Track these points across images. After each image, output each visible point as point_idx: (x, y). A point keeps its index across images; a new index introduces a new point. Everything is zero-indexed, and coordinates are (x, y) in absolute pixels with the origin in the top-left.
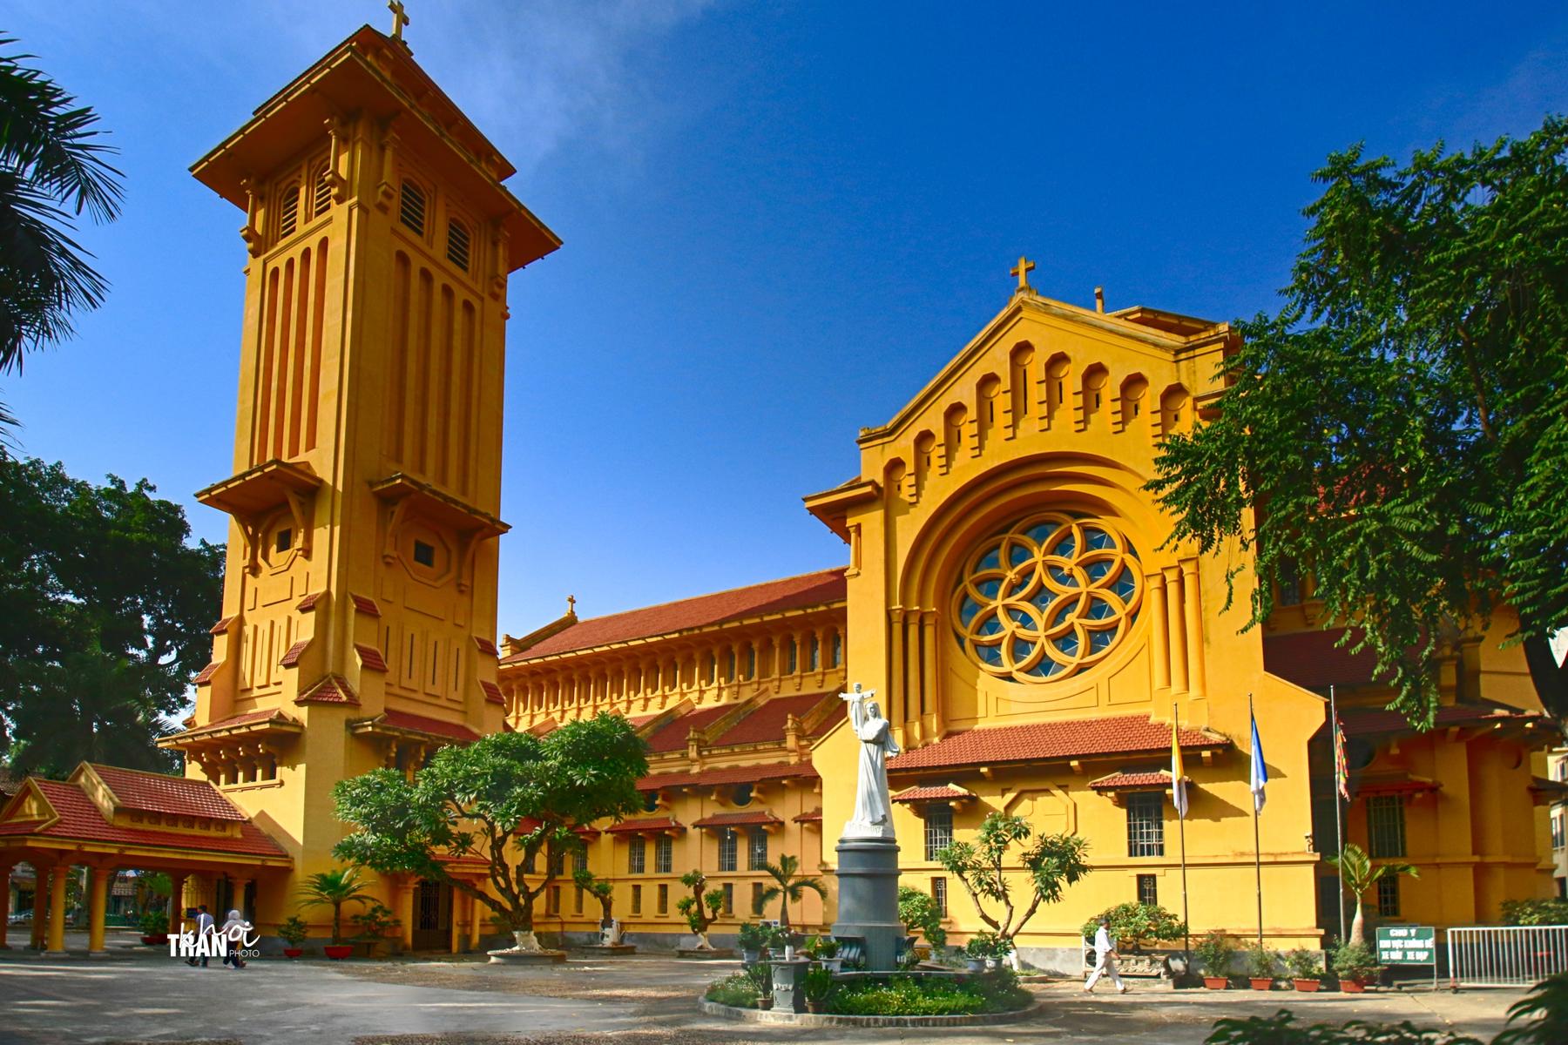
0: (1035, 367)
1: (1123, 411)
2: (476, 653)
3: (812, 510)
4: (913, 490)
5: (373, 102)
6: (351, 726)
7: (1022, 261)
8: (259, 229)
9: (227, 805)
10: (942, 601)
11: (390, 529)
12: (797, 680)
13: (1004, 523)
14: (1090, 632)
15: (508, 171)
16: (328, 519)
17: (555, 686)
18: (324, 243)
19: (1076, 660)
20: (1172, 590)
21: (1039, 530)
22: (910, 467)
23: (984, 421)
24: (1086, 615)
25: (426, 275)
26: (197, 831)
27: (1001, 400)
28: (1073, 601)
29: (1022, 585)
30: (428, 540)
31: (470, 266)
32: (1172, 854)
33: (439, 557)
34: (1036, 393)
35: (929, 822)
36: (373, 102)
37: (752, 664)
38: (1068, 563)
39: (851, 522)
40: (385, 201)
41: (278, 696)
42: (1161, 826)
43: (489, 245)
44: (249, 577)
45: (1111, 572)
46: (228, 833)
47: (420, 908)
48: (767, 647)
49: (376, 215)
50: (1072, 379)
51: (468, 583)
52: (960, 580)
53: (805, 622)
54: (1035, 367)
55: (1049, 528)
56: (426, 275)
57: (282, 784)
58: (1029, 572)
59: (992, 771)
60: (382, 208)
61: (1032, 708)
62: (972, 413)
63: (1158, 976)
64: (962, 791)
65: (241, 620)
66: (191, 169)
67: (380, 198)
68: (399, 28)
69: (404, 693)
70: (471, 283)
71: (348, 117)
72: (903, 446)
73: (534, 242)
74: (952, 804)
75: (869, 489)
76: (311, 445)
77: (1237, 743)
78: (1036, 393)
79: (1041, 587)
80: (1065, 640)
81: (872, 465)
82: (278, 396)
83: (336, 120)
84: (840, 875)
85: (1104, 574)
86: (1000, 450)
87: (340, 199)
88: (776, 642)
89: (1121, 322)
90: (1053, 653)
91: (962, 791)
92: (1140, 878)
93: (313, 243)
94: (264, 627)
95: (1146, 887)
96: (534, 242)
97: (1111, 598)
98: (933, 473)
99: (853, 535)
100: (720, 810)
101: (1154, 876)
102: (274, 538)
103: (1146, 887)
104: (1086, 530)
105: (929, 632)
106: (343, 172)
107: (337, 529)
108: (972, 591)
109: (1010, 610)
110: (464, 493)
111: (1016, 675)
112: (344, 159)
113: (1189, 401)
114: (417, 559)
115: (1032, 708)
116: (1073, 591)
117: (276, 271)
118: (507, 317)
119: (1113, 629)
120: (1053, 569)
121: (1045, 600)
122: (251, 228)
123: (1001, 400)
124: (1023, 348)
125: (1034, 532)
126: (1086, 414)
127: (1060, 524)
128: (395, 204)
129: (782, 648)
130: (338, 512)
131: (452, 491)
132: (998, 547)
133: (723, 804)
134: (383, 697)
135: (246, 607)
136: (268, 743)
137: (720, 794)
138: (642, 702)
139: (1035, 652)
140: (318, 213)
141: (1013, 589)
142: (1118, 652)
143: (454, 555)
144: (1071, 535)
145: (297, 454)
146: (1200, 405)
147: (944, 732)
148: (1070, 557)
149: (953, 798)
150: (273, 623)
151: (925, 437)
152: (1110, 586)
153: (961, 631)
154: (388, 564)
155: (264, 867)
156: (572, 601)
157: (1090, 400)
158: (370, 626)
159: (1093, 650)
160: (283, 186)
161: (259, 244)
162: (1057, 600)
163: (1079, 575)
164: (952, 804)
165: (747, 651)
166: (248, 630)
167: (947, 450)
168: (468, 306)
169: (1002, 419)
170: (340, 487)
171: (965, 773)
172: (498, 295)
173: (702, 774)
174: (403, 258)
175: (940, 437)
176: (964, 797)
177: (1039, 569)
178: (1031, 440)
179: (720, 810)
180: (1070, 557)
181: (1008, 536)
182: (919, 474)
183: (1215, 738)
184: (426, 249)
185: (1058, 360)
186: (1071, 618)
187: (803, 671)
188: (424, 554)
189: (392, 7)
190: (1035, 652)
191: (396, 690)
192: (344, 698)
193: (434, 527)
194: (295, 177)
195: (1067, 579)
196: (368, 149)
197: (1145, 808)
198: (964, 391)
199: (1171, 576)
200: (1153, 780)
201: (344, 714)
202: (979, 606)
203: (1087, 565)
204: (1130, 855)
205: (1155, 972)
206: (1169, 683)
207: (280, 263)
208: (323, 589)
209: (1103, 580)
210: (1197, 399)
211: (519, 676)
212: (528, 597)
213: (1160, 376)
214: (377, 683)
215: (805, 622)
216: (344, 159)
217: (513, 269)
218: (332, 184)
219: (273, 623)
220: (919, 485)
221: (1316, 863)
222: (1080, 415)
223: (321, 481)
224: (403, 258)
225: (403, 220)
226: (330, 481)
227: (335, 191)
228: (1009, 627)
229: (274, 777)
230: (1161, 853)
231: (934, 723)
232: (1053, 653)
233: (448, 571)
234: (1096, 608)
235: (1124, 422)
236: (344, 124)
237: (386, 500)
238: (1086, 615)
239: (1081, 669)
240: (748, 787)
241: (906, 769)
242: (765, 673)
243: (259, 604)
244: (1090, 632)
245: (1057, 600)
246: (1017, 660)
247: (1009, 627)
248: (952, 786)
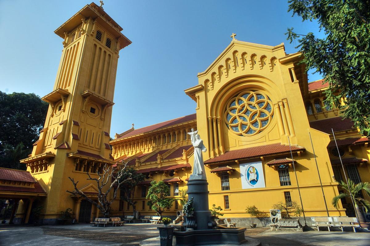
0: (239, 56)
1: (262, 64)
2: (104, 136)
3: (186, 93)
4: (212, 87)
5: (93, 15)
6: (68, 154)
7: (233, 34)
8: (66, 42)
9: (33, 179)
10: (222, 115)
11: (85, 103)
12: (187, 141)
13: (236, 94)
14: (261, 121)
15: (121, 29)
16: (70, 100)
17: (127, 145)
18: (79, 43)
19: (259, 129)
20: (281, 107)
21: (244, 95)
22: (211, 81)
23: (228, 68)
24: (260, 116)
25: (100, 49)
26: (21, 186)
27: (231, 64)
28: (256, 113)
29: (242, 110)
30: (94, 107)
31: (111, 47)
32: (294, 184)
33: (96, 111)
34: (240, 61)
35: (222, 178)
36: (93, 15)
37: (175, 138)
38: (254, 103)
39: (197, 95)
40: (93, 34)
41: (51, 148)
42: (288, 175)
43: (116, 43)
44: (51, 117)
45: (265, 105)
46: (30, 187)
47: (83, 210)
48: (179, 133)
49: (90, 37)
50: (248, 57)
51: (103, 118)
52: (226, 109)
53: (187, 124)
54: (239, 56)
56: (100, 49)
57: (48, 172)
59: (239, 161)
60: (92, 35)
61: (248, 143)
62: (225, 67)
63: (297, 227)
64: (231, 168)
65: (47, 129)
66: (54, 32)
67: (91, 33)
68: (101, 5)
69: (84, 146)
70: (111, 51)
71: (87, 18)
72: (209, 76)
73: (125, 42)
74: (228, 172)
75: (200, 87)
76: (69, 85)
77: (306, 149)
78: (240, 61)
79: (247, 110)
80: (255, 123)
81: (201, 81)
82: (64, 76)
83: (84, 19)
84: (188, 185)
85: (263, 105)
86: (232, 75)
87: (83, 34)
88: (181, 131)
90: (252, 127)
91: (231, 168)
92: (285, 192)
93: (76, 43)
94: (52, 130)
95: (287, 196)
96: (125, 42)
97: (266, 112)
98: (216, 82)
99: (197, 99)
100: (166, 178)
102: (58, 108)
103: (287, 196)
104: (257, 95)
106: (84, 29)
107: (72, 103)
108: (229, 111)
110: (104, 95)
111: (243, 134)
112: (85, 25)
113: (277, 60)
114: (91, 112)
115: (248, 143)
116: (255, 110)
117: (68, 50)
118: (119, 58)
121: (248, 113)
122: (65, 42)
123: (231, 64)
124: (235, 52)
125: (243, 96)
126: (253, 65)
128: (95, 35)
129: (183, 133)
130: (72, 100)
131: (101, 95)
132: (235, 100)
133: (166, 176)
134: (78, 147)
135: (49, 125)
136: (46, 160)
137: (165, 173)
138: (148, 149)
139: (247, 127)
140: (78, 38)
142: (269, 126)
143: (100, 111)
144: (253, 96)
145: (66, 88)
146: (281, 61)
147: (225, 151)
148: (254, 102)
149: (228, 170)
150: (54, 128)
151: (214, 74)
152: (265, 108)
153: (227, 123)
154: (83, 113)
155: (38, 196)
156: (133, 125)
157: (253, 63)
158: (77, 128)
159: (262, 126)
160: (73, 33)
161: (66, 45)
162: (252, 113)
163: (257, 106)
164: (228, 172)
165: (174, 134)
166: (48, 131)
167: (220, 76)
168: (110, 55)
169: (232, 68)
170: (73, 95)
171: (232, 163)
172: (117, 53)
173: (162, 168)
174: (95, 45)
175: (217, 73)
176: (231, 170)
177: (246, 105)
178: (240, 72)
179: (166, 178)
180: (254, 102)
181: (237, 97)
182: (213, 82)
183: (300, 147)
184: (101, 44)
185: (244, 54)
186: (256, 117)
188: (93, 111)
189: (100, 2)
190: (247, 127)
191: (82, 145)
192: (67, 147)
193: (96, 102)
194: (75, 31)
196: (90, 24)
197: (283, 170)
198: (222, 62)
199: (281, 104)
200: (285, 161)
201: (66, 152)
203: (258, 103)
204: (281, 185)
205: (296, 226)
206: (285, 133)
207: (69, 48)
208: (66, 119)
209: (263, 107)
210: (279, 59)
211: (118, 144)
212: (119, 124)
213: (269, 55)
214: (77, 143)
215: (187, 124)
216: (85, 25)
217: (121, 48)
218: (82, 31)
219: (54, 128)
220: (213, 85)
221: (338, 185)
222: (251, 66)
223: (70, 93)
224: (95, 45)
225: (96, 38)
226: (72, 94)
227: (82, 32)
228: (240, 121)
229: (46, 170)
230: (290, 184)
231: (221, 148)
232: (252, 127)
233: (98, 115)
234: (262, 114)
235: (262, 66)
236: (86, 20)
237: (84, 97)
238: (260, 116)
239: (260, 131)
240: (173, 171)
241: (215, 162)
242: (179, 140)
243: (52, 124)
244: (261, 121)
245: (252, 113)
246: (243, 130)
247: (240, 121)
248: (228, 167)
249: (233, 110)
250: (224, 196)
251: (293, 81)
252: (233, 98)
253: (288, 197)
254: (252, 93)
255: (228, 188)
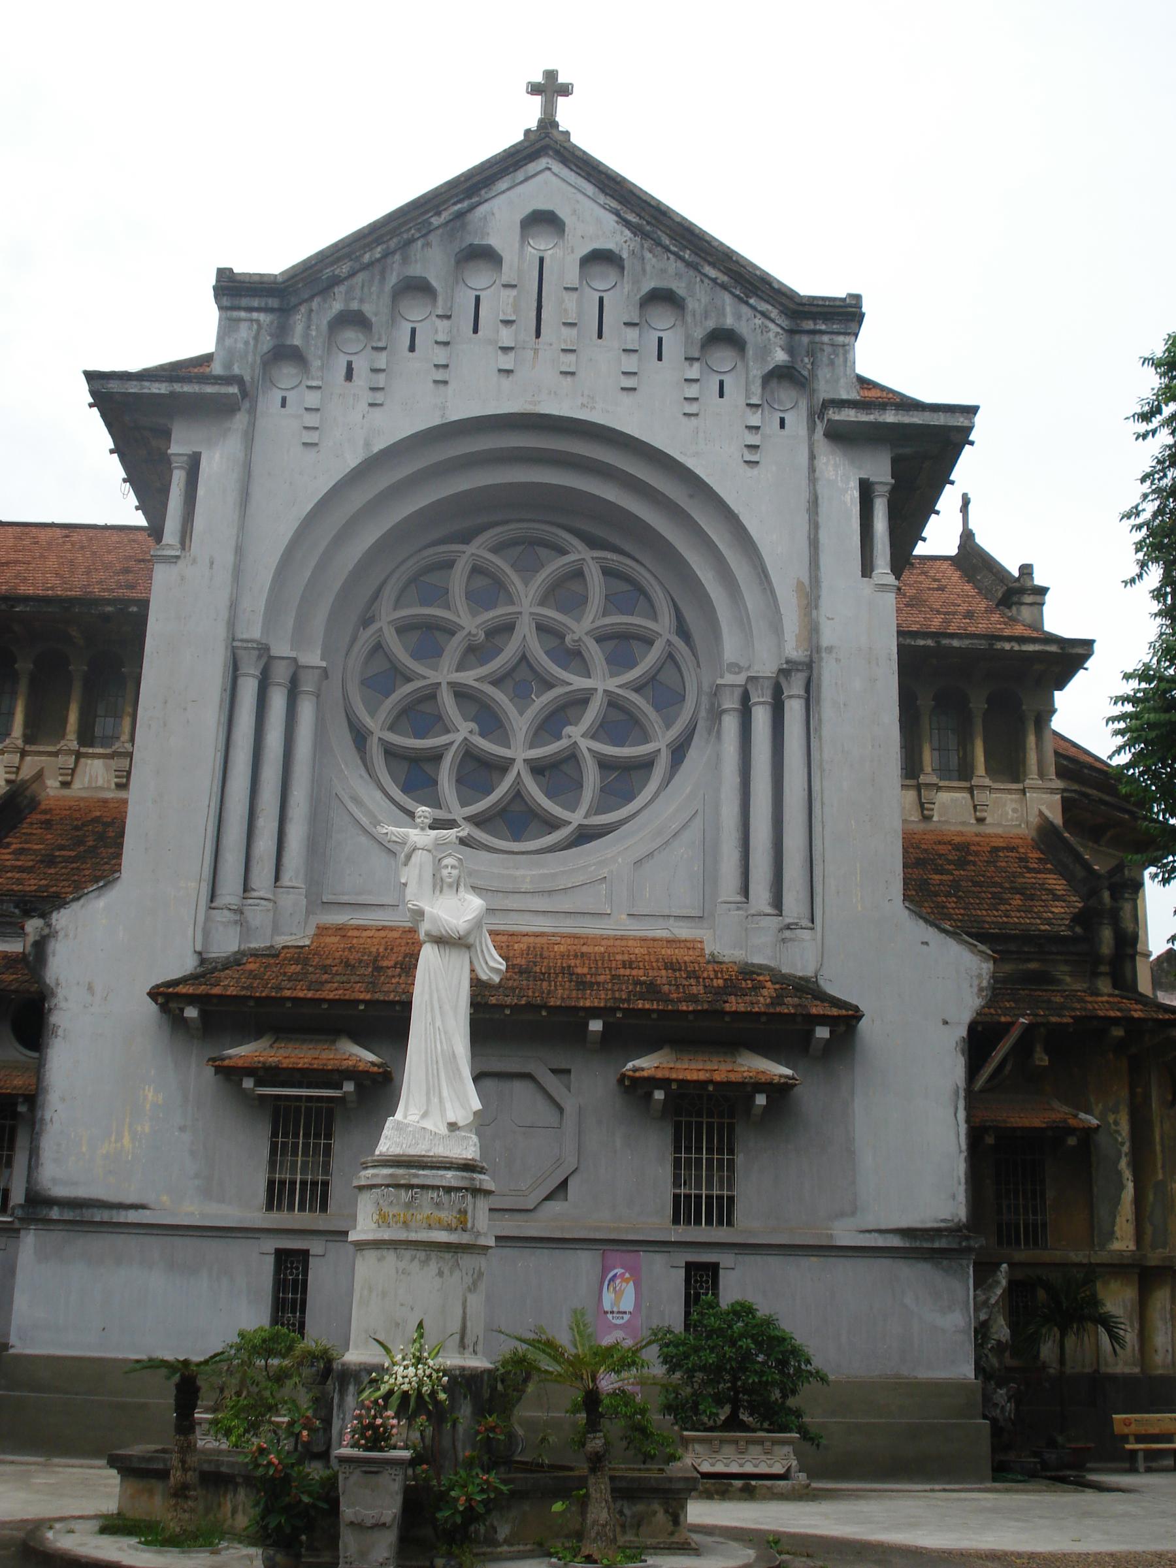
19: (576, 818)
52: (466, 538)
55: (543, 552)
58: (507, 628)
89: (461, 613)
97: (591, 777)
101: (305, 1255)
105: (306, 711)
109: (462, 694)
119: (646, 765)
120: (491, 721)
127: (563, 552)
141: (475, 653)
146: (835, 415)
148: (578, 620)
163: (595, 653)
180: (578, 620)
181: (472, 549)
186: (576, 734)
187: (28, 739)
195: (573, 657)
202: (441, 596)
238: (603, 730)
239: (584, 836)
245: (559, 691)
249: (566, 591)
250: (689, 1266)
251: (867, 569)
252: (560, 526)
253: (295, 1281)
254: (580, 553)
255: (722, 1211)
